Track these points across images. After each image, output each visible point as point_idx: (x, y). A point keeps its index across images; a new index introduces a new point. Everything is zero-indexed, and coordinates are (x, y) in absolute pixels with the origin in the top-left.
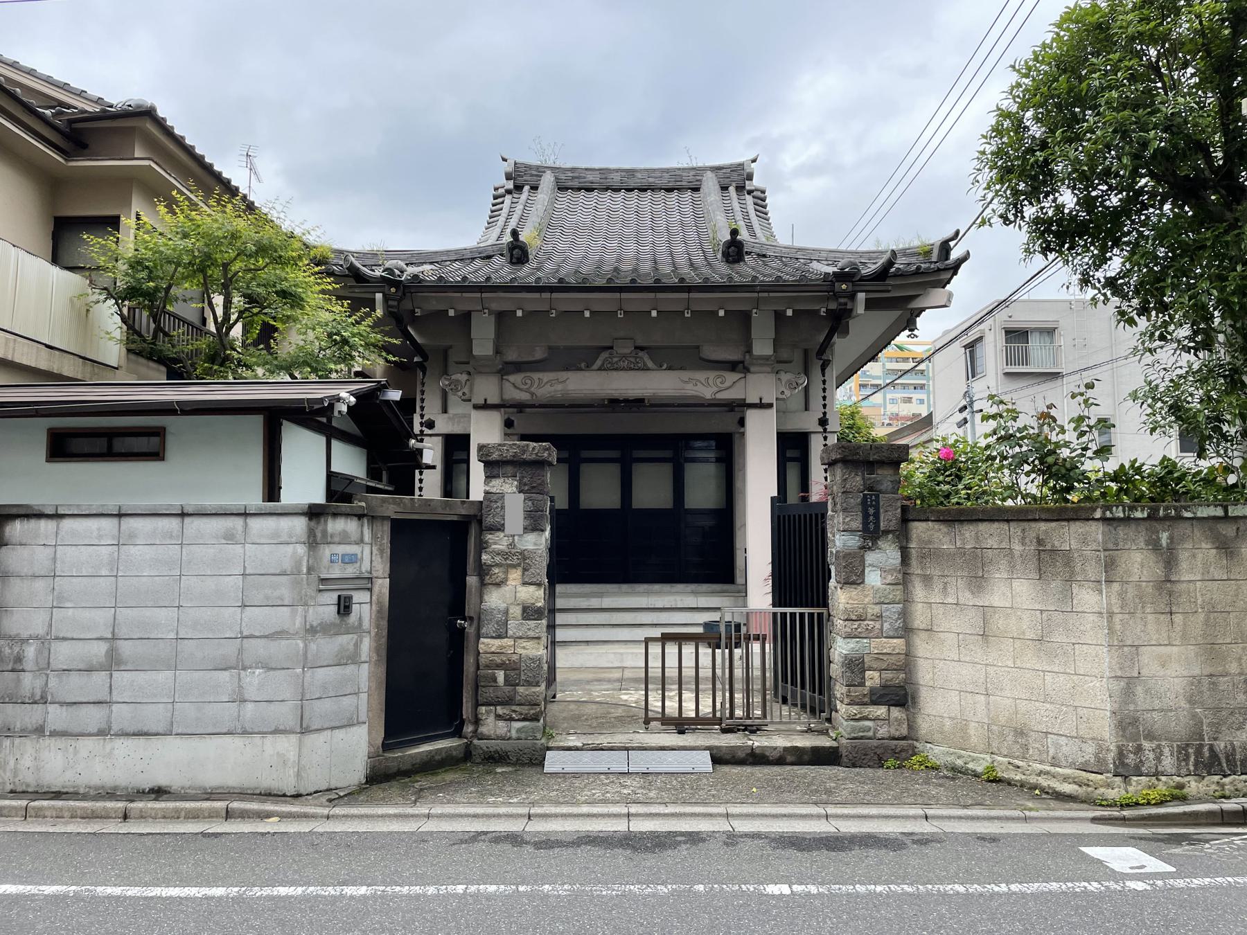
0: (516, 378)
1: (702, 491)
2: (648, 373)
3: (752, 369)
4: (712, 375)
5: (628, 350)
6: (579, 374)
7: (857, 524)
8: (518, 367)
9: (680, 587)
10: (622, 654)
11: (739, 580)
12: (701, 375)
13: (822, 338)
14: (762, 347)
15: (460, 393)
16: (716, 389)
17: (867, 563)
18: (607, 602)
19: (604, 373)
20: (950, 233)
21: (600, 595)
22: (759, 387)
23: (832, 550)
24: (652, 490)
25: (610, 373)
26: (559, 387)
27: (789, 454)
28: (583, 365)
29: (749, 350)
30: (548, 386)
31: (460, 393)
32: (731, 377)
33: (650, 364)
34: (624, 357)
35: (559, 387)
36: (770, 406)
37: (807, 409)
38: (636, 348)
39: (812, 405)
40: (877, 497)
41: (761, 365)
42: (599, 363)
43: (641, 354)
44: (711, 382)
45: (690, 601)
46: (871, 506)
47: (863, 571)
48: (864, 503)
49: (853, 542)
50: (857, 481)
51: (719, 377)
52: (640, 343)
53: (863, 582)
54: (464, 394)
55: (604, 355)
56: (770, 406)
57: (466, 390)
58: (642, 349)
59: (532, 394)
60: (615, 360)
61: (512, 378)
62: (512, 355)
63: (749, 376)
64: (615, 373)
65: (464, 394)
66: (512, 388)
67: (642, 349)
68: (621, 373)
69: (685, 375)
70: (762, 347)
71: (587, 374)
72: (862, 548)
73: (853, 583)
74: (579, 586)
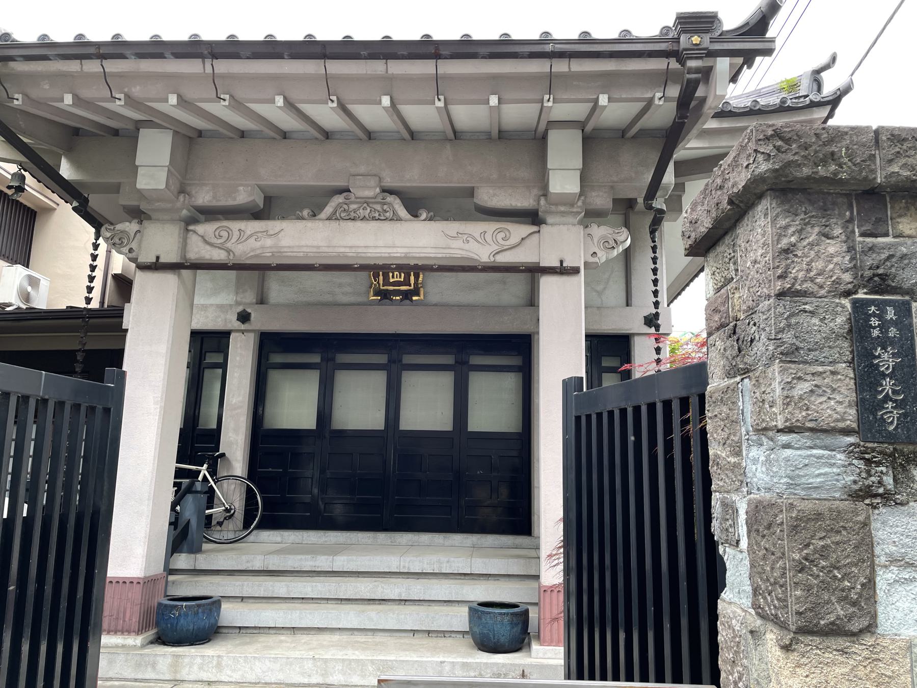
0: (206, 229)
1: (491, 409)
2: (398, 225)
3: (550, 220)
4: (490, 227)
5: (371, 192)
6: (300, 224)
7: (838, 403)
8: (210, 214)
9: (457, 539)
10: (326, 661)
11: (535, 531)
12: (476, 228)
13: (648, 177)
14: (564, 181)
15: (125, 250)
16: (495, 248)
17: (881, 552)
18: (341, 562)
19: (334, 224)
20: (824, 60)
21: (334, 550)
22: (561, 242)
23: (733, 510)
24: (427, 405)
25: (343, 224)
26: (269, 242)
27: (607, 362)
28: (306, 213)
29: (545, 191)
30: (252, 240)
31: (125, 250)
32: (519, 231)
33: (403, 212)
34: (366, 202)
35: (269, 242)
36: (575, 271)
37: (628, 304)
38: (384, 191)
39: (635, 300)
40: (904, 310)
41: (563, 214)
42: (328, 210)
43: (390, 198)
44: (488, 237)
45: (460, 564)
46: (884, 342)
47: (870, 584)
48: (858, 329)
49: (829, 470)
50: (828, 255)
51: (501, 230)
52: (389, 182)
53: (870, 628)
54: (131, 250)
55: (339, 199)
56: (575, 271)
57: (134, 245)
58: (391, 192)
59: (229, 251)
60: (353, 207)
61: (201, 229)
62: (204, 198)
63: (544, 229)
64: (350, 224)
65: (131, 250)
66: (201, 244)
67: (391, 192)
68: (359, 224)
69: (453, 227)
70: (564, 181)
71: (309, 224)
72: (862, 494)
73: (835, 631)
74: (321, 533)
